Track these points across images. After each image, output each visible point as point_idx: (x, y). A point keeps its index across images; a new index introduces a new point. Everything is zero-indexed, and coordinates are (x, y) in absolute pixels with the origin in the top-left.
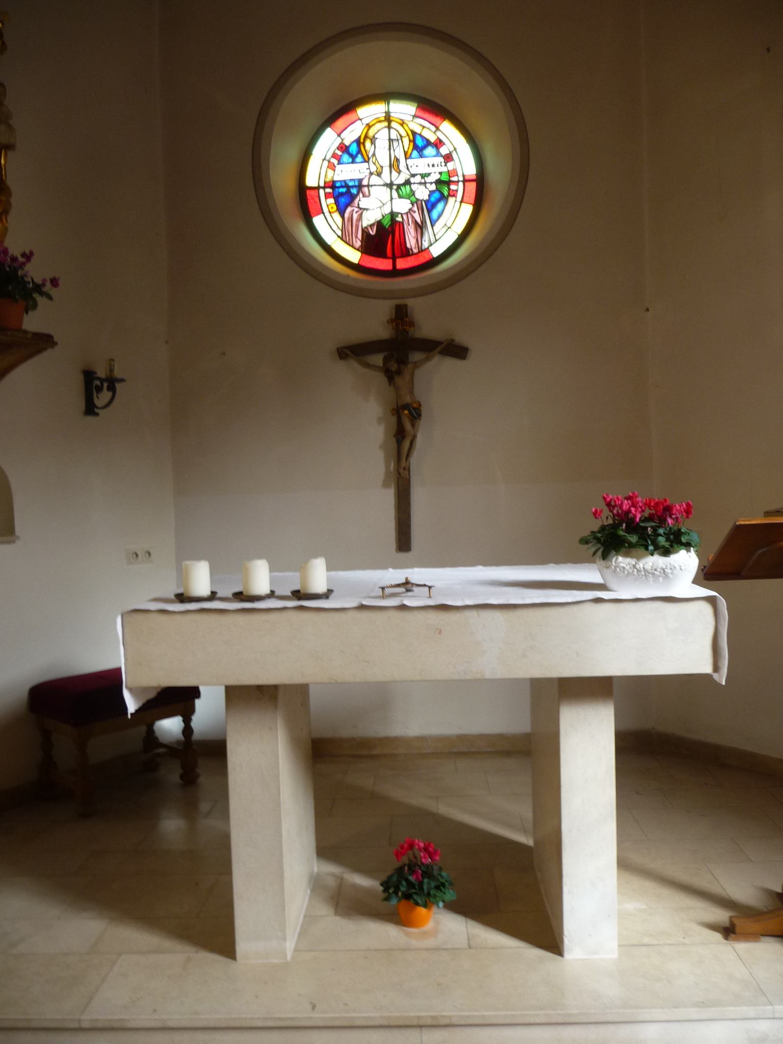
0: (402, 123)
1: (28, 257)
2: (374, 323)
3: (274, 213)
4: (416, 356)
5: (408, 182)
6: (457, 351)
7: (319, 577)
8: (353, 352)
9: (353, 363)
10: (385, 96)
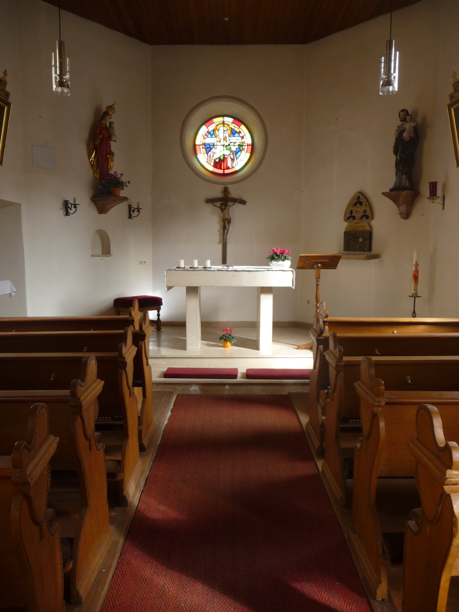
1: (122, 175)
2: (217, 192)
3: (186, 154)
4: (230, 204)
5: (229, 145)
6: (243, 202)
7: (208, 264)
8: (210, 201)
9: (210, 205)
10: (223, 116)
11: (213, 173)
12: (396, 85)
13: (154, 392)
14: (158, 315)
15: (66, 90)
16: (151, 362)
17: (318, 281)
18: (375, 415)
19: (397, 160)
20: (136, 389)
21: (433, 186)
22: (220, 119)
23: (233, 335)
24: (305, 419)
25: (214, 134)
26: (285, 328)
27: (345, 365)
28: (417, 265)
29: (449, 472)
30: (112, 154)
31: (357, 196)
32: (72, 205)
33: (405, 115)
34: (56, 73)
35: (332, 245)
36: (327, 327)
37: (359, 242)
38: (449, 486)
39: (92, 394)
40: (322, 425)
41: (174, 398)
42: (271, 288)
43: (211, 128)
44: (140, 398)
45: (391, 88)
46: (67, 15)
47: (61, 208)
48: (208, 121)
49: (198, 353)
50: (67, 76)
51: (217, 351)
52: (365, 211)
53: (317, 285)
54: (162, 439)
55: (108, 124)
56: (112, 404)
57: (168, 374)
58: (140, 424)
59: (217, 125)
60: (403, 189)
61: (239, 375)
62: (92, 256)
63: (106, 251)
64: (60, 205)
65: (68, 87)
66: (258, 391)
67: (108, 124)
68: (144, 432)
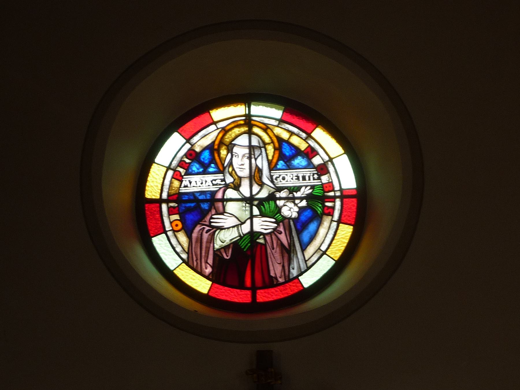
0: (266, 128)
5: (272, 197)
10: (247, 99)
25: (212, 160)
59: (225, 131)
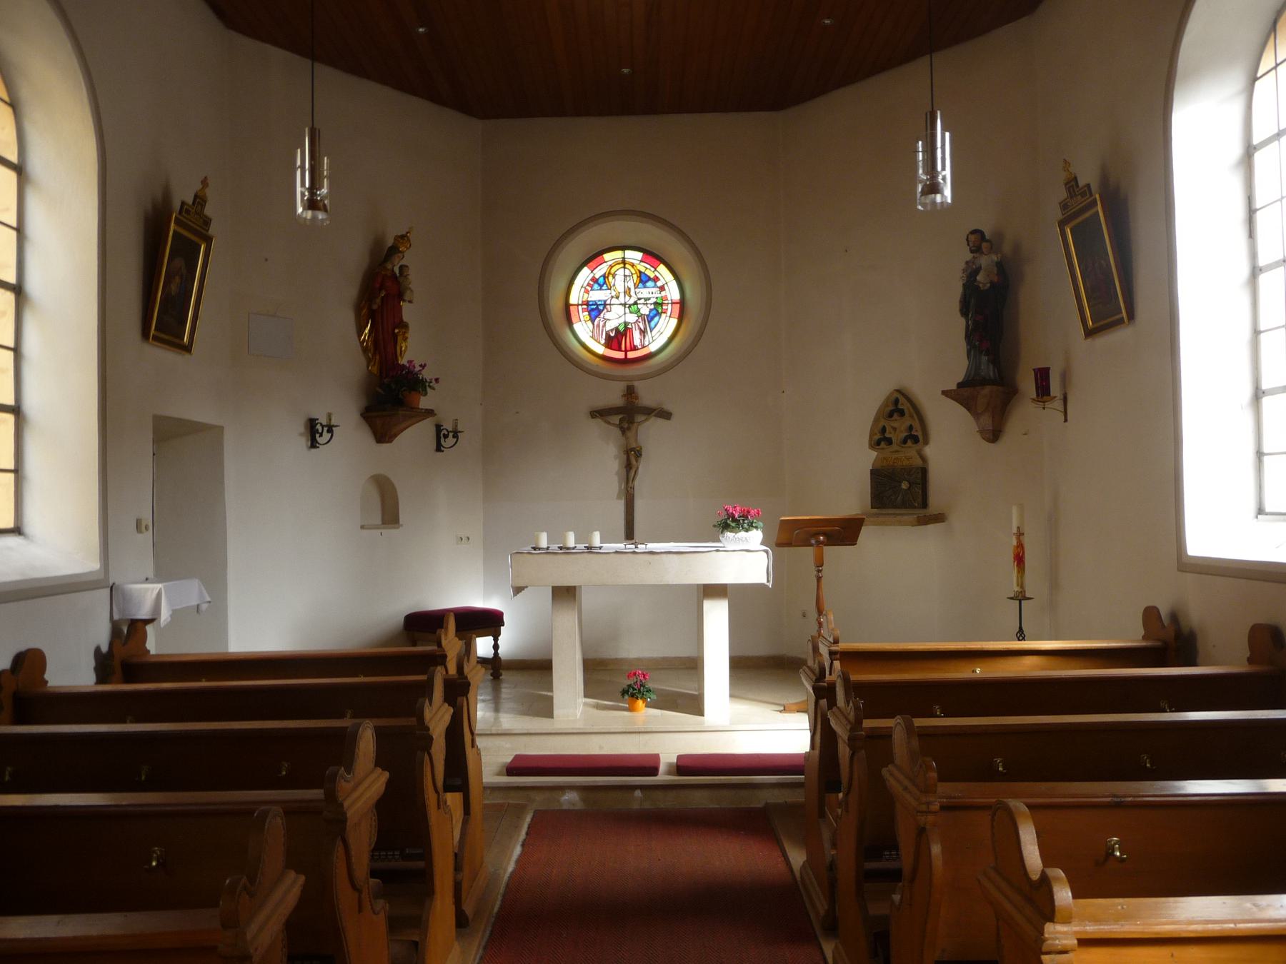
0: (633, 265)
1: (423, 366)
2: (612, 396)
3: (550, 323)
4: (639, 418)
5: (636, 303)
6: (666, 415)
7: (596, 539)
8: (600, 413)
9: (599, 421)
10: (623, 248)
11: (604, 358)
12: (948, 192)
13: (486, 807)
14: (496, 647)
15: (321, 215)
16: (480, 742)
17: (819, 571)
18: (922, 831)
19: (967, 326)
20: (449, 796)
21: (1042, 376)
22: (618, 254)
23: (650, 685)
24: (797, 858)
26: (751, 669)
27: (868, 737)
28: (1020, 534)
29: (1049, 928)
30: (404, 326)
31: (893, 398)
32: (323, 426)
33: (978, 241)
34: (303, 184)
35: (846, 493)
36: (837, 664)
37: (901, 490)
38: (1052, 956)
39: (368, 795)
40: (832, 867)
41: (528, 819)
42: (725, 586)
43: (599, 272)
44: (458, 814)
45: (938, 198)
46: (325, 72)
47: (301, 435)
48: (593, 258)
49: (577, 722)
50: (325, 191)
51: (618, 718)
52: (911, 428)
53: (819, 579)
54: (503, 901)
55: (397, 270)
56: (402, 820)
57: (511, 770)
58: (458, 868)
59: (611, 267)
60: (984, 382)
61: (662, 768)
62: (362, 527)
63: (390, 517)
64: (301, 427)
65: (325, 209)
66: (701, 801)
67: (397, 270)
68: (465, 886)
